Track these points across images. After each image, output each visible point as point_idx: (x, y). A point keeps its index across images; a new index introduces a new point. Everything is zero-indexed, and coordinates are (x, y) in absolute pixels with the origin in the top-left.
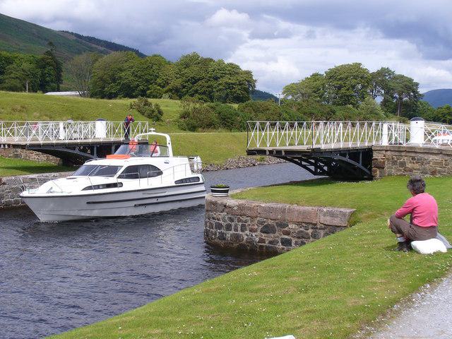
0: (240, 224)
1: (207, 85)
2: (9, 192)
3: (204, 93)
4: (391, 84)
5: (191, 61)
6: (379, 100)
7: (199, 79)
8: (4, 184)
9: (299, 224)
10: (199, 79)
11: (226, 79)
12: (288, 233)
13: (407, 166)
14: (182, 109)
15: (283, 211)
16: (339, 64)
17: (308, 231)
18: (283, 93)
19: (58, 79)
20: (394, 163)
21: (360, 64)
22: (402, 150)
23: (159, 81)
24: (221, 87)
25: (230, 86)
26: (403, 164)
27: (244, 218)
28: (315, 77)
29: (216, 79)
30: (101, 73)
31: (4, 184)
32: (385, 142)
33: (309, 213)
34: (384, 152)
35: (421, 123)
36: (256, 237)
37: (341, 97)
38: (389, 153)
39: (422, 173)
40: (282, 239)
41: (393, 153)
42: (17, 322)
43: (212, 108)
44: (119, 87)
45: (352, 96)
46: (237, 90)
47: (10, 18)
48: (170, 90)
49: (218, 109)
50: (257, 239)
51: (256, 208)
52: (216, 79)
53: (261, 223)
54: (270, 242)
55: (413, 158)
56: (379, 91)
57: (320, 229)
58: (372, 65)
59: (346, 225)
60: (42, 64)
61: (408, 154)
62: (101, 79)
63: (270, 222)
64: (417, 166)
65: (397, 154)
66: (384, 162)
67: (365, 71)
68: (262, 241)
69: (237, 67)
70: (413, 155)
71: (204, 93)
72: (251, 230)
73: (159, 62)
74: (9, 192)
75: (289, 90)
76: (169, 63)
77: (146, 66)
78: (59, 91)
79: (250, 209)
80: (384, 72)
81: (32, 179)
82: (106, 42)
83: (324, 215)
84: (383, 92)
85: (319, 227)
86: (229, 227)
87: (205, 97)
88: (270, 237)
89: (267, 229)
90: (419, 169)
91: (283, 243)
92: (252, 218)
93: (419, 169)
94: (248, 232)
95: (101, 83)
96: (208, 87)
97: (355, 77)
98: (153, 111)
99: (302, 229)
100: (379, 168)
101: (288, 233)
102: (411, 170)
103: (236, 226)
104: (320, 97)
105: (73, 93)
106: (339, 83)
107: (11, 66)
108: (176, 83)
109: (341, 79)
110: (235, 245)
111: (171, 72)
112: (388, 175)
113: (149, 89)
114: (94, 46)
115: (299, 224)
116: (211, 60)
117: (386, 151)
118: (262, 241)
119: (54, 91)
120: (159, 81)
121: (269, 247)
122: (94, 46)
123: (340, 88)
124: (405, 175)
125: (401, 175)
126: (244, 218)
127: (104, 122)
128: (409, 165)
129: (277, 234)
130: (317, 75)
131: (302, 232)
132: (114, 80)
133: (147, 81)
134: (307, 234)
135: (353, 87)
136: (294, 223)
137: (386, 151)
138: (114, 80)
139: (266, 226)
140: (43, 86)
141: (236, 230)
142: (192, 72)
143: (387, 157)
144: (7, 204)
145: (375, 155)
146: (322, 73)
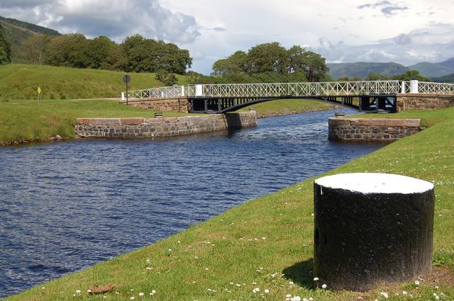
9: (393, 127)
12: (387, 132)
15: (385, 121)
20: (409, 103)
21: (278, 43)
26: (414, 103)
27: (362, 127)
28: (239, 54)
33: (399, 121)
35: (417, 81)
36: (369, 135)
42: (226, 190)
46: (176, 65)
48: (119, 67)
64: (423, 104)
68: (373, 137)
69: (176, 47)
77: (95, 47)
79: (366, 121)
82: (26, 23)
86: (353, 132)
97: (274, 55)
101: (387, 132)
108: (124, 61)
115: (393, 127)
118: (373, 137)
126: (362, 127)
141: (357, 132)
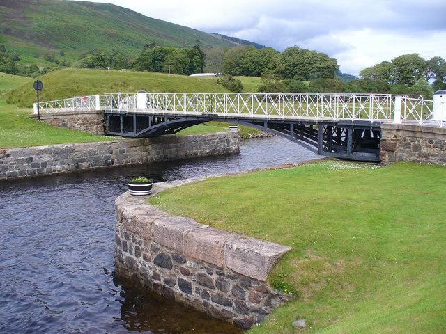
0: (134, 245)
1: (303, 68)
2: (13, 164)
3: (301, 74)
4: (441, 68)
5: (292, 52)
6: (431, 81)
7: (298, 65)
8: (8, 156)
9: (199, 262)
10: (298, 65)
11: (317, 65)
12: (186, 273)
13: (422, 150)
14: (262, 84)
16: (401, 54)
17: (212, 277)
18: (360, 75)
19: (203, 64)
20: (407, 145)
21: (418, 54)
22: (416, 130)
23: (269, 65)
24: (313, 70)
25: (320, 69)
26: (417, 148)
28: (384, 63)
29: (310, 64)
30: (229, 60)
31: (8, 156)
32: (397, 120)
34: (395, 132)
37: (403, 79)
38: (401, 133)
39: (441, 160)
40: (180, 279)
41: (406, 133)
43: (286, 83)
44: (241, 70)
45: (411, 78)
47: (139, 16)
48: (278, 72)
49: (291, 84)
50: (151, 273)
51: (149, 226)
52: (310, 64)
53: (155, 250)
54: (166, 281)
55: (431, 141)
56: (431, 75)
57: (229, 277)
58: (427, 56)
59: (264, 280)
60: (191, 55)
61: (424, 136)
62: (229, 64)
63: (165, 251)
64: (434, 151)
65: (411, 134)
66: (394, 145)
67: (421, 59)
68: (156, 276)
70: (430, 137)
71: (301, 74)
72: (145, 258)
73: (271, 52)
74: (13, 164)
75: (364, 72)
76: (278, 53)
78: (203, 72)
80: (436, 60)
81: (40, 150)
83: (233, 257)
84: (435, 75)
85: (226, 273)
87: (302, 77)
88: (165, 274)
89: (162, 261)
90: (437, 156)
91: (181, 287)
92: (147, 240)
93: (437, 156)
94: (141, 259)
95: (229, 67)
96: (304, 70)
98: (235, 86)
99: (204, 272)
100: (388, 151)
101: (186, 273)
102: (427, 156)
103: (131, 246)
104: (387, 78)
105: (211, 74)
106: (402, 68)
107: (168, 56)
108: (281, 67)
109: (403, 65)
110: (130, 274)
111: (276, 59)
112: (399, 161)
113: (262, 71)
114: (234, 43)
115: (199, 262)
116: (307, 51)
117: (398, 130)
119: (199, 73)
120: (269, 65)
121: (163, 288)
122: (234, 43)
123: (402, 72)
124: (419, 161)
125: (414, 161)
127: (145, 94)
128: (425, 150)
129: (173, 271)
130: (386, 62)
131: (203, 275)
132: (238, 65)
133: (261, 66)
134: (211, 281)
135: (412, 71)
136: (193, 259)
137: (398, 130)
138: (238, 65)
139: (161, 256)
140: (191, 71)
142: (294, 59)
143: (399, 138)
144: (10, 176)
145: (385, 136)
146: (389, 60)
